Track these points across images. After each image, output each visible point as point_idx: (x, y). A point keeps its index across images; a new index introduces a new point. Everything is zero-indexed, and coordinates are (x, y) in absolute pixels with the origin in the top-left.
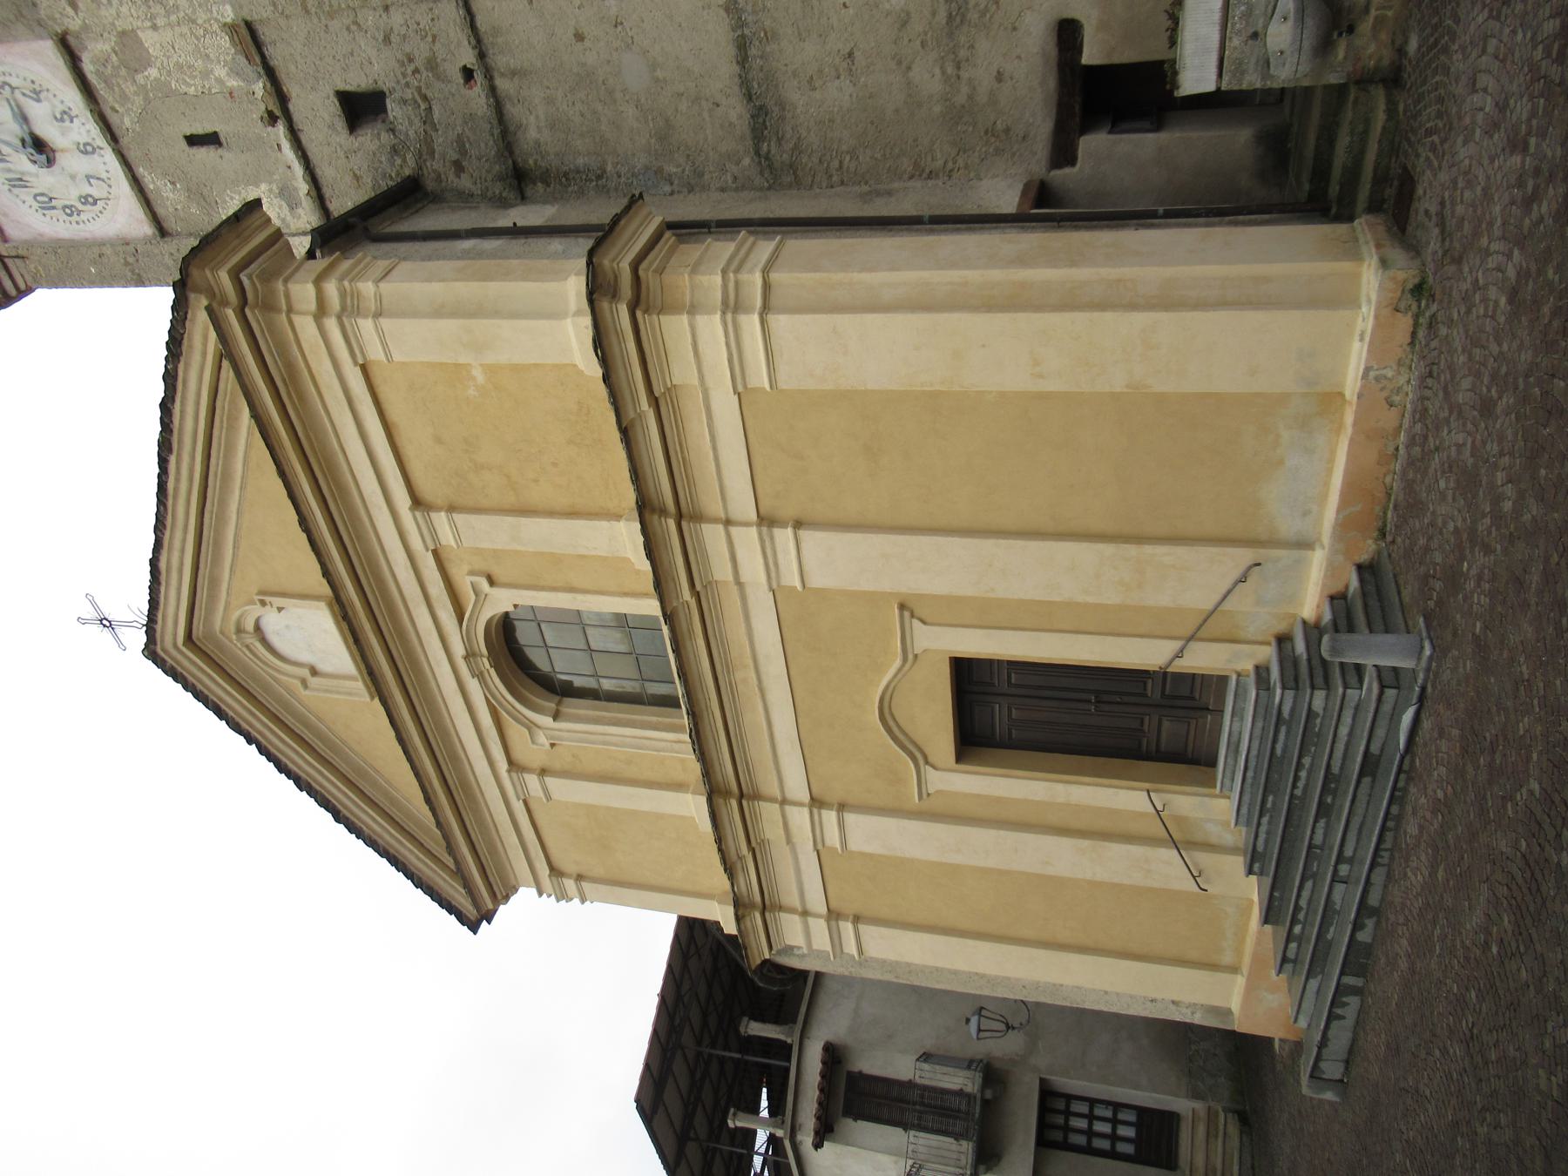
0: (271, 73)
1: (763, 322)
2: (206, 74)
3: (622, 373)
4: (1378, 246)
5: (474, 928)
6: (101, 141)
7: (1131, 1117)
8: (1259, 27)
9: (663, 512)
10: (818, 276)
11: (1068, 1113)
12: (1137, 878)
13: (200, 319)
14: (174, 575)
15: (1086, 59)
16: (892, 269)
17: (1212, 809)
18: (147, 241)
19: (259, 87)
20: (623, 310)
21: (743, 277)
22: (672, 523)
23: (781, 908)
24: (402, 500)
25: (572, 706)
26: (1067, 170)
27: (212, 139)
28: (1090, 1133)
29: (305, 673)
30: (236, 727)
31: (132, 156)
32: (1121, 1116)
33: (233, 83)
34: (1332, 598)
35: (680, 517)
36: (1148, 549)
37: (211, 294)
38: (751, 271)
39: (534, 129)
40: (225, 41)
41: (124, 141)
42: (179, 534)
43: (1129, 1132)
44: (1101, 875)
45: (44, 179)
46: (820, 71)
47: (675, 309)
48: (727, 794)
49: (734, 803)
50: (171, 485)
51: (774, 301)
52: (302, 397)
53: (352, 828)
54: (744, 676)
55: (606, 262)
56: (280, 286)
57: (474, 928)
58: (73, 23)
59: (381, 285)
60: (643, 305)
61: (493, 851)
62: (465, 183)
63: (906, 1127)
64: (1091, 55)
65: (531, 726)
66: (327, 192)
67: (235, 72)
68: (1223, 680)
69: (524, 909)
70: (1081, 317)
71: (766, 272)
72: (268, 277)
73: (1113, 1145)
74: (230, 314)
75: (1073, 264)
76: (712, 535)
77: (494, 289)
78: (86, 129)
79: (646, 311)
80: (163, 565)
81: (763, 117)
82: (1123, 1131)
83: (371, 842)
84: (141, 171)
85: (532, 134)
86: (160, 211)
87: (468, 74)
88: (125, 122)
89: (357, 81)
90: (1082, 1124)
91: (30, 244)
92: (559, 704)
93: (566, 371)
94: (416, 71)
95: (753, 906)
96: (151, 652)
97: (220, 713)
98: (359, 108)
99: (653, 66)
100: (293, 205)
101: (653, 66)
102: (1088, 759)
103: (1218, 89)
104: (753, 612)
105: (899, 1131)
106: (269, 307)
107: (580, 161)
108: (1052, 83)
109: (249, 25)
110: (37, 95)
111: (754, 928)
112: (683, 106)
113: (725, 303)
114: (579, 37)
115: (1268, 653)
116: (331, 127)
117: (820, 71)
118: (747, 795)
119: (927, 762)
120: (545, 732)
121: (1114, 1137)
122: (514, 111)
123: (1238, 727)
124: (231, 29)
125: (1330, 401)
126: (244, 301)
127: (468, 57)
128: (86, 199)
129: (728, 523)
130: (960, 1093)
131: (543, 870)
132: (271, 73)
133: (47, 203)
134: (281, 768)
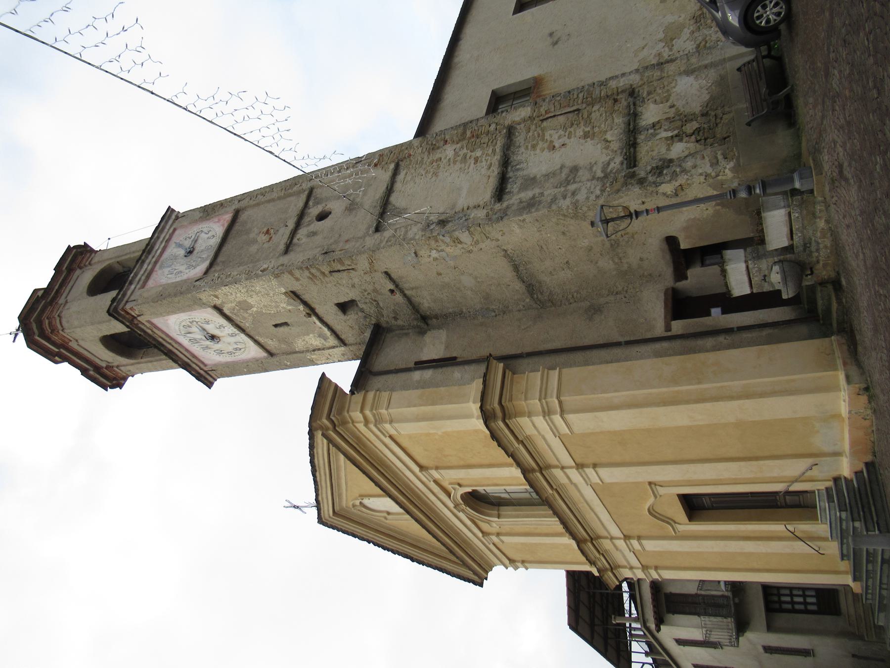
0: (305, 303)
1: (562, 418)
2: (278, 307)
3: (505, 440)
4: (845, 364)
5: (481, 585)
6: (235, 331)
7: (813, 593)
8: (766, 273)
9: (533, 470)
10: (583, 397)
11: (779, 595)
12: (788, 551)
13: (319, 435)
14: (325, 500)
15: (682, 247)
16: (616, 391)
17: (821, 528)
18: (265, 358)
19: (301, 307)
20: (501, 424)
21: (549, 400)
22: (538, 474)
23: (619, 567)
24: (416, 469)
25: (505, 510)
26: (684, 282)
27: (286, 324)
28: (793, 603)
29: (385, 515)
30: (362, 539)
31: (252, 334)
32: (807, 593)
33: (289, 307)
34: (856, 473)
35: (541, 470)
36: (762, 462)
37: (321, 428)
38: (552, 397)
39: (426, 303)
40: (283, 297)
41: (247, 331)
42: (324, 490)
43: (813, 600)
44: (769, 551)
45: (217, 346)
46: (555, 270)
47: (521, 414)
48: (585, 541)
49: (590, 544)
50: (318, 479)
51: (565, 407)
52: (364, 445)
53: (420, 562)
54: (583, 506)
55: (488, 407)
56: (346, 414)
57: (481, 585)
58: (218, 302)
59: (390, 410)
60: (507, 416)
61: (482, 558)
62: (400, 322)
63: (699, 615)
64: (683, 246)
65: (489, 522)
66: (339, 333)
67: (288, 304)
68: (814, 492)
69: (498, 575)
70: (708, 405)
71: (558, 398)
72: (340, 412)
73: (806, 607)
74: (332, 433)
75: (699, 383)
76: (557, 472)
77: (438, 408)
78: (230, 329)
79: (510, 418)
80: (320, 498)
81: (532, 287)
82: (809, 600)
83: (429, 565)
84: (257, 338)
85: (426, 305)
86: (268, 348)
87: (392, 291)
88: (247, 325)
89: (342, 300)
90: (788, 599)
91: (215, 365)
92: (498, 510)
93: (477, 431)
94: (369, 294)
95: (606, 570)
96: (321, 521)
97: (354, 536)
98: (344, 307)
99: (476, 278)
100: (325, 339)
101: (476, 278)
102: (753, 511)
103: (752, 292)
104: (582, 491)
105: (696, 617)
106: (344, 423)
107: (451, 310)
108: (668, 257)
109: (293, 292)
110: (208, 323)
111: (609, 577)
112: (493, 288)
113: (544, 412)
114: (439, 274)
115: (830, 484)
116: (336, 314)
117: (555, 270)
118: (594, 539)
119: (675, 522)
120: (493, 523)
121: (805, 603)
122: (416, 300)
123: (822, 504)
124: (285, 293)
125: (837, 416)
126: (334, 426)
127: (392, 287)
128: (236, 349)
129: (563, 468)
130: (723, 596)
131: (507, 562)
132: (305, 303)
133: (220, 352)
134: (384, 548)
